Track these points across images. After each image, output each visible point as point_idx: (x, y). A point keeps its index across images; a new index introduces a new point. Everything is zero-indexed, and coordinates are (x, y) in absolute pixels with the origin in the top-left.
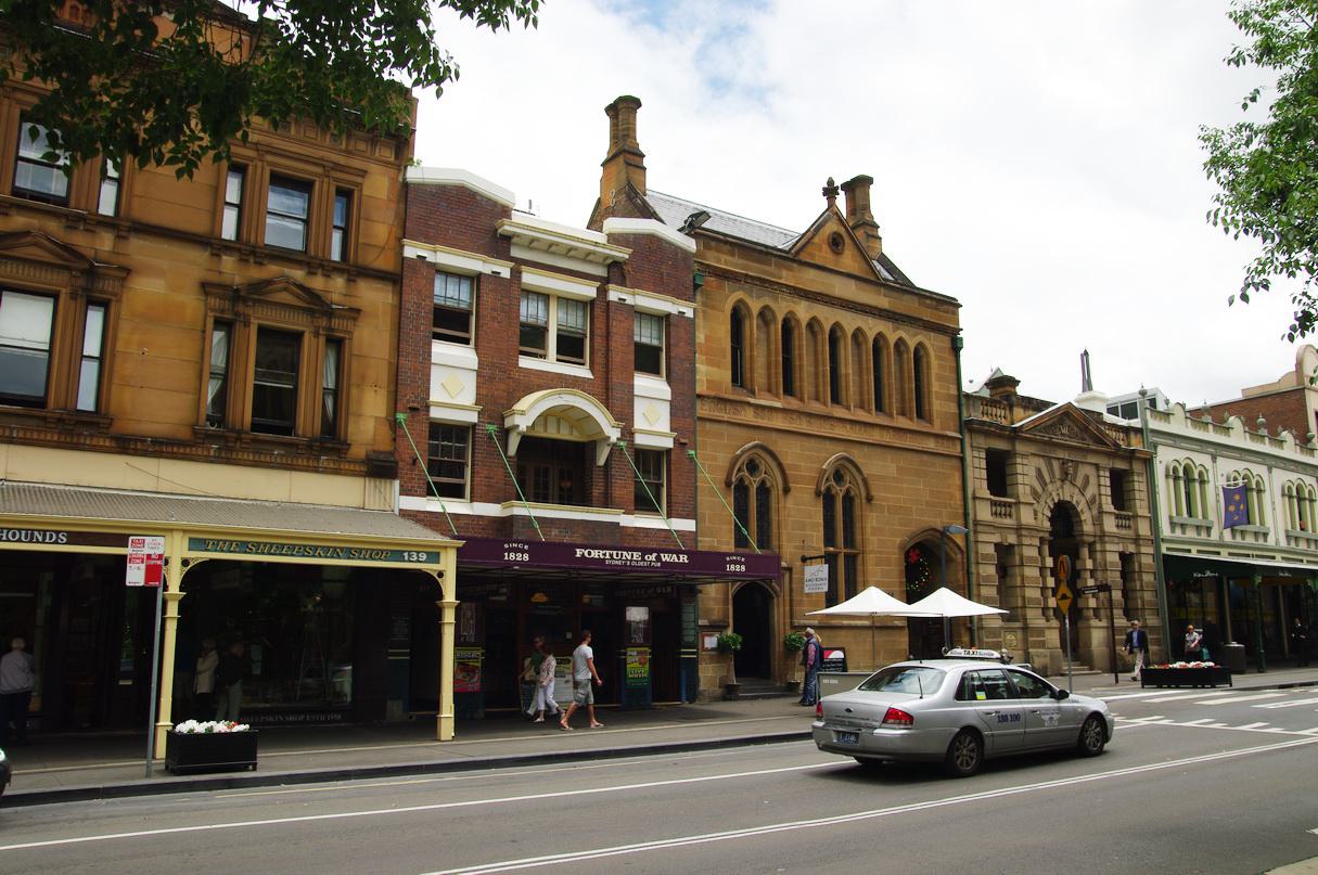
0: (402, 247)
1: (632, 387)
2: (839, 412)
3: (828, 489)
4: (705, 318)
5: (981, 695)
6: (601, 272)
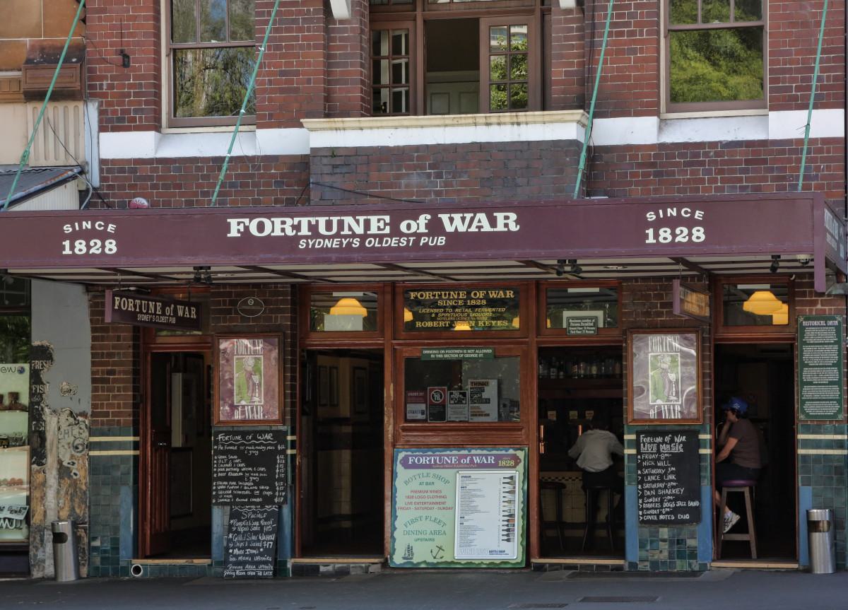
5: (228, 287)
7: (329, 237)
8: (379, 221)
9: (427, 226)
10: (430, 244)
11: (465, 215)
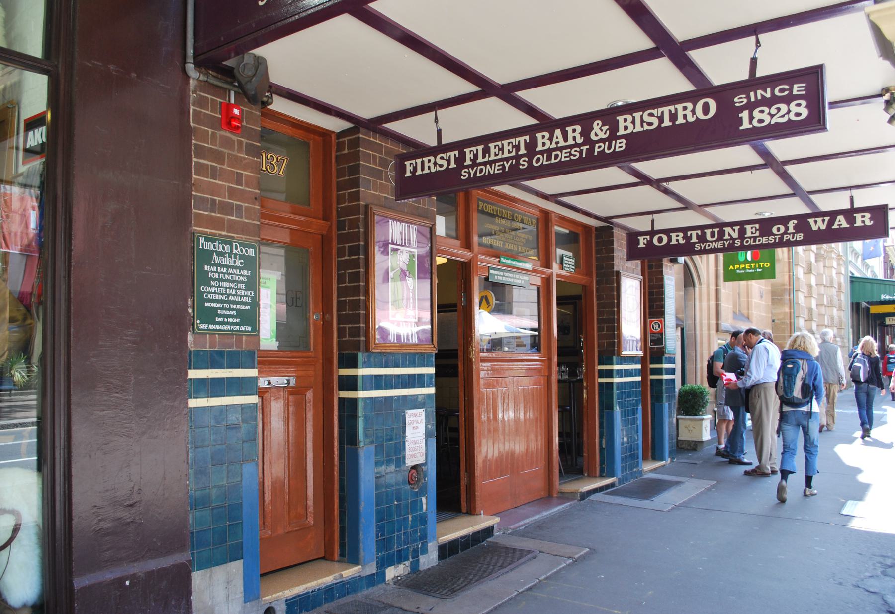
7: (715, 241)
9: (794, 228)
10: (607, 151)
11: (825, 218)
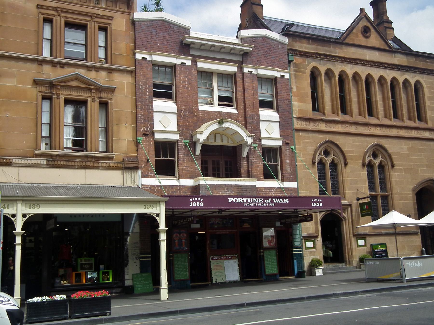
0: (134, 54)
1: (259, 116)
2: (373, 121)
3: (370, 162)
4: (295, 78)
6: (239, 59)
7: (251, 203)
8: (261, 200)
9: (271, 201)
